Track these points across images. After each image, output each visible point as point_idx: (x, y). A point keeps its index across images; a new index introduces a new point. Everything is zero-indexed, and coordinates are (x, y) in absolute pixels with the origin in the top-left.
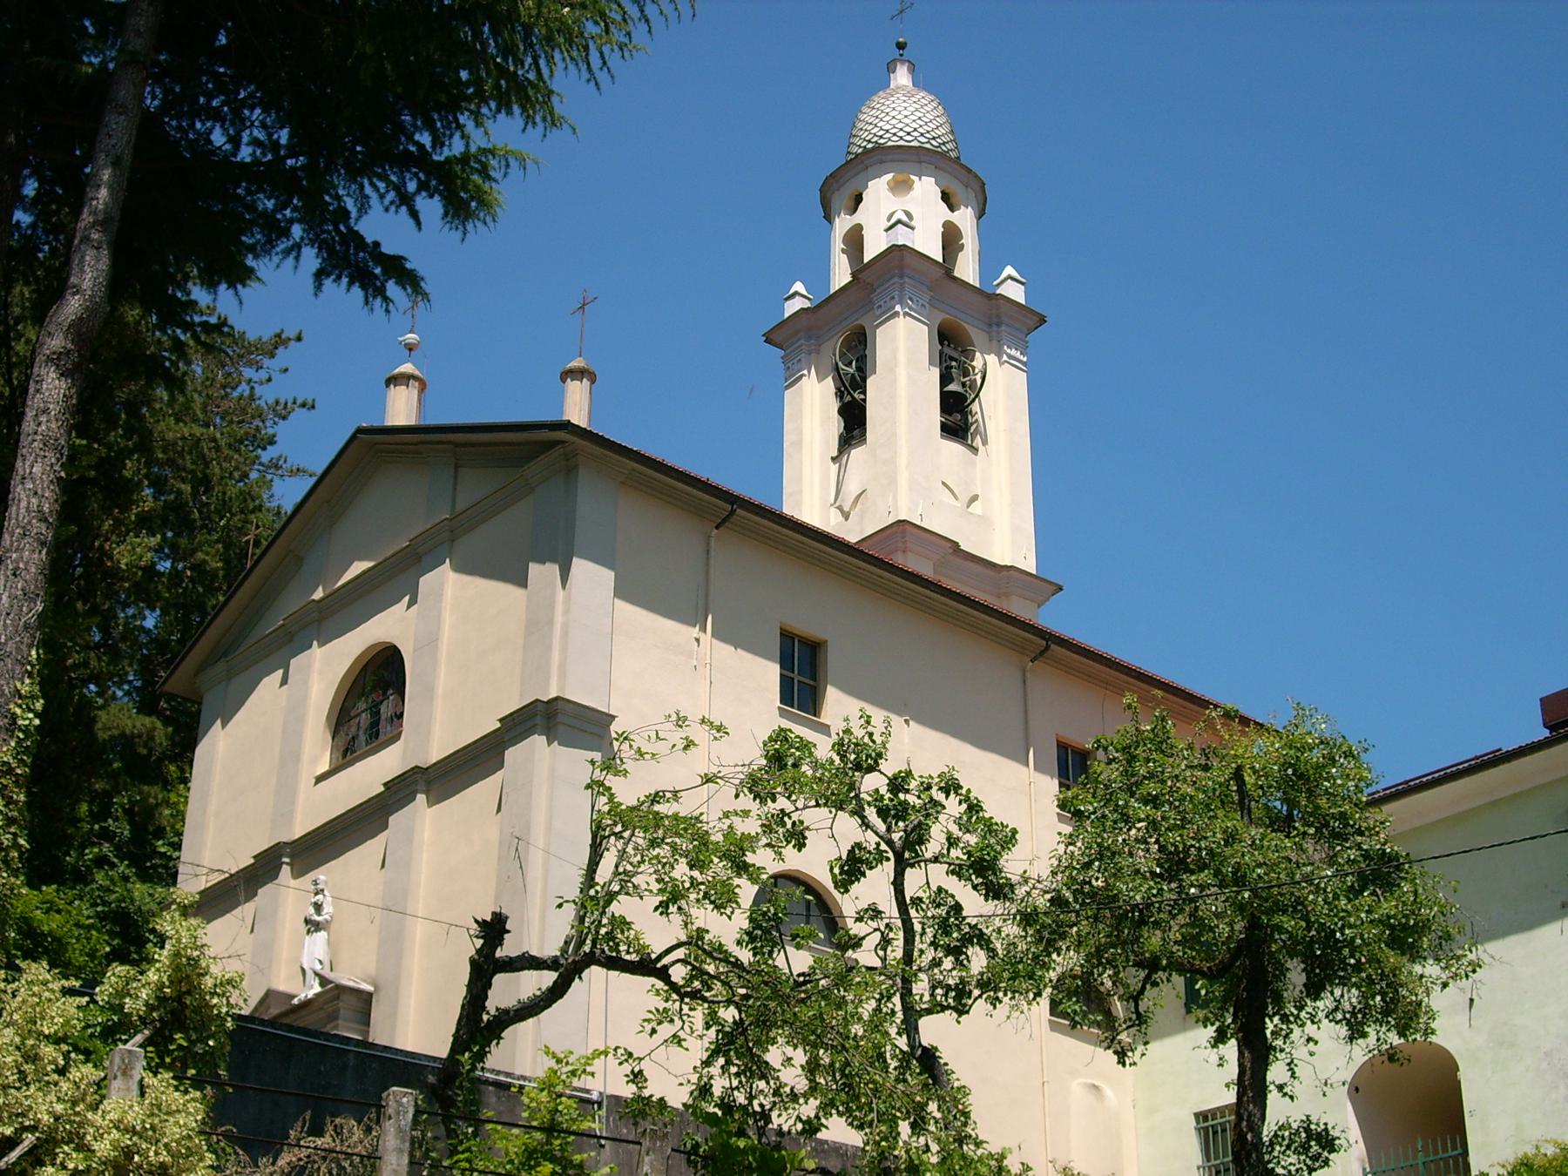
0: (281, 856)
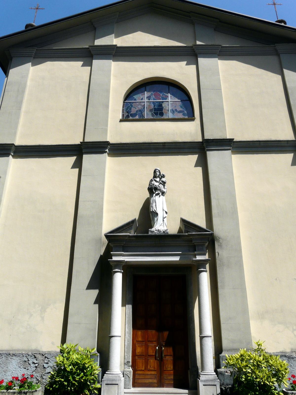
0: (106, 148)
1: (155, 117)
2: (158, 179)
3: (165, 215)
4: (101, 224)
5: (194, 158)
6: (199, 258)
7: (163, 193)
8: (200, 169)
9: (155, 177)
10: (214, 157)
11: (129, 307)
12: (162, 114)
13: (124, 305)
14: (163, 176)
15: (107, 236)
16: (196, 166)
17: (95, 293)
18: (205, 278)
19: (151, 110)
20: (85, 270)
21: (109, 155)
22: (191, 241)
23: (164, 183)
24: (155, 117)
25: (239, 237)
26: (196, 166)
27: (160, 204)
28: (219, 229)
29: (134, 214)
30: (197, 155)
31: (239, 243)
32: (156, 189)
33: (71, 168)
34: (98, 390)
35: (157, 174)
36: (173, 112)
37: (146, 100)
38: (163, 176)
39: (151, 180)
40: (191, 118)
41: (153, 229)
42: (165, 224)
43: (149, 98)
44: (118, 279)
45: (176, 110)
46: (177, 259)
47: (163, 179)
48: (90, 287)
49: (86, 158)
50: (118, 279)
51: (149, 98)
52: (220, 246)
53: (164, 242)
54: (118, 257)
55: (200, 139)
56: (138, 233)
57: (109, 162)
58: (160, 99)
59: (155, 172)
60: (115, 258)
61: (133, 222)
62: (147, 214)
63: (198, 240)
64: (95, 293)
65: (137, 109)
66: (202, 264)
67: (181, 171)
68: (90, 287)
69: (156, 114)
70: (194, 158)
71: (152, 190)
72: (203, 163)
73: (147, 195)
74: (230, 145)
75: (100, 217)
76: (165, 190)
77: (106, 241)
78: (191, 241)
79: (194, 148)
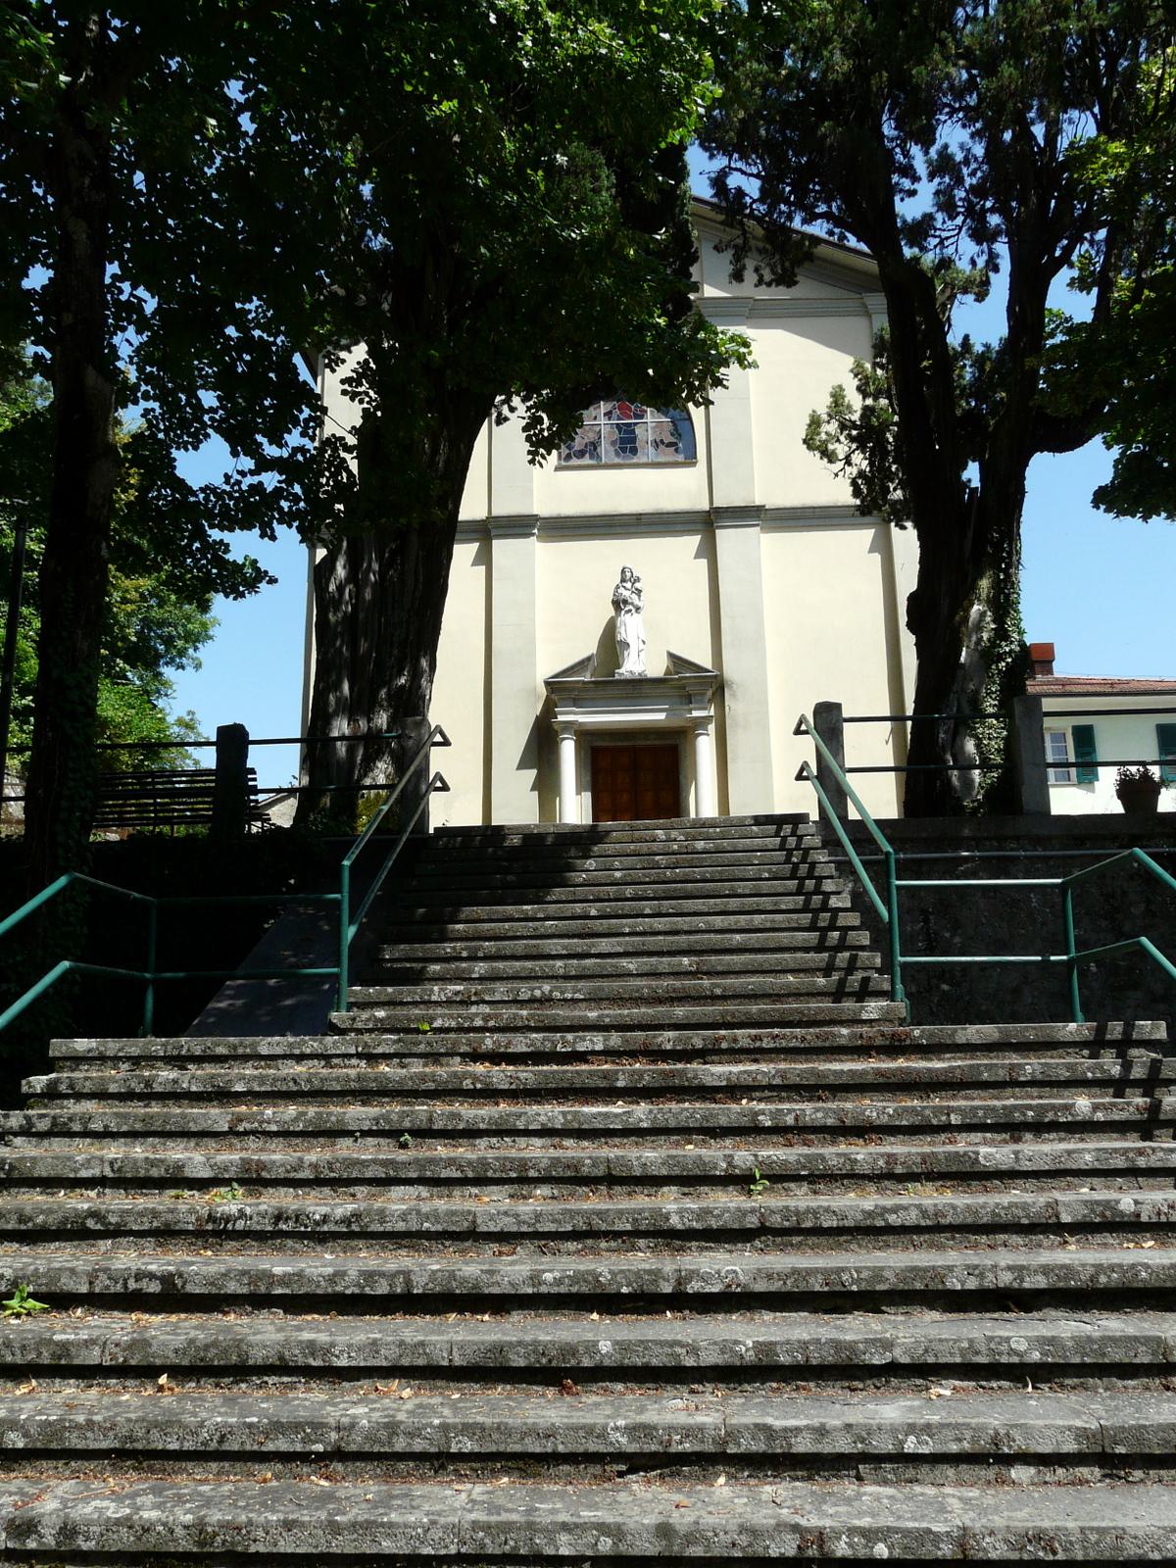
1: (617, 460)
2: (628, 585)
3: (642, 646)
4: (534, 665)
5: (694, 541)
6: (695, 714)
7: (638, 609)
8: (704, 562)
9: (623, 580)
10: (725, 538)
11: (587, 796)
12: (634, 451)
13: (578, 792)
14: (638, 580)
15: (547, 684)
16: (697, 556)
17: (531, 774)
18: (705, 747)
19: (613, 443)
20: (513, 738)
21: (540, 538)
22: (684, 687)
23: (639, 592)
24: (617, 460)
25: (765, 682)
26: (697, 556)
27: (631, 628)
28: (733, 669)
29: (589, 646)
30: (698, 538)
31: (765, 692)
32: (625, 602)
33: (519, 767)
34: (713, 175)
35: (626, 577)
36: (656, 444)
37: (603, 421)
38: (638, 580)
39: (618, 587)
40: (691, 460)
41: (620, 671)
42: (642, 661)
43: (608, 414)
44: (568, 750)
45: (662, 441)
46: (662, 716)
47: (637, 585)
48: (523, 765)
49: (499, 546)
50: (568, 750)
51: (608, 414)
52: (734, 695)
53: (639, 689)
54: (565, 716)
55: (706, 507)
56: (600, 675)
57: (537, 550)
58: (630, 417)
59: (623, 572)
60: (561, 718)
61: (589, 659)
62: (611, 645)
63: (697, 686)
64: (531, 774)
65: (587, 440)
66: (702, 723)
67: (671, 561)
68: (523, 765)
69: (624, 450)
70: (694, 541)
71: (619, 604)
72: (708, 550)
73: (612, 612)
74: (758, 517)
75: (532, 654)
76: (640, 604)
77: (543, 691)
78: (684, 687)
79: (693, 522)
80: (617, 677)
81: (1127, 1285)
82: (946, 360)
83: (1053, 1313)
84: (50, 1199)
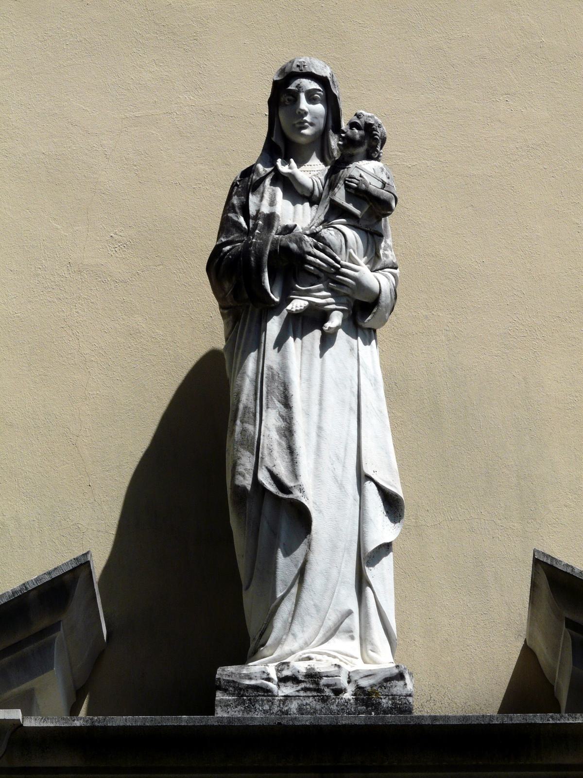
2: (311, 172)
3: (382, 529)
9: (281, 144)
14: (368, 141)
23: (370, 212)
27: (330, 417)
38: (368, 141)
39: (247, 183)
41: (261, 669)
47: (367, 171)
59: (282, 94)
61: (59, 591)
71: (254, 277)
73: (203, 325)
76: (378, 281)
80: (226, 710)
81: (376, 724)
82: (372, 265)
83: (275, 618)
84: (224, 353)
